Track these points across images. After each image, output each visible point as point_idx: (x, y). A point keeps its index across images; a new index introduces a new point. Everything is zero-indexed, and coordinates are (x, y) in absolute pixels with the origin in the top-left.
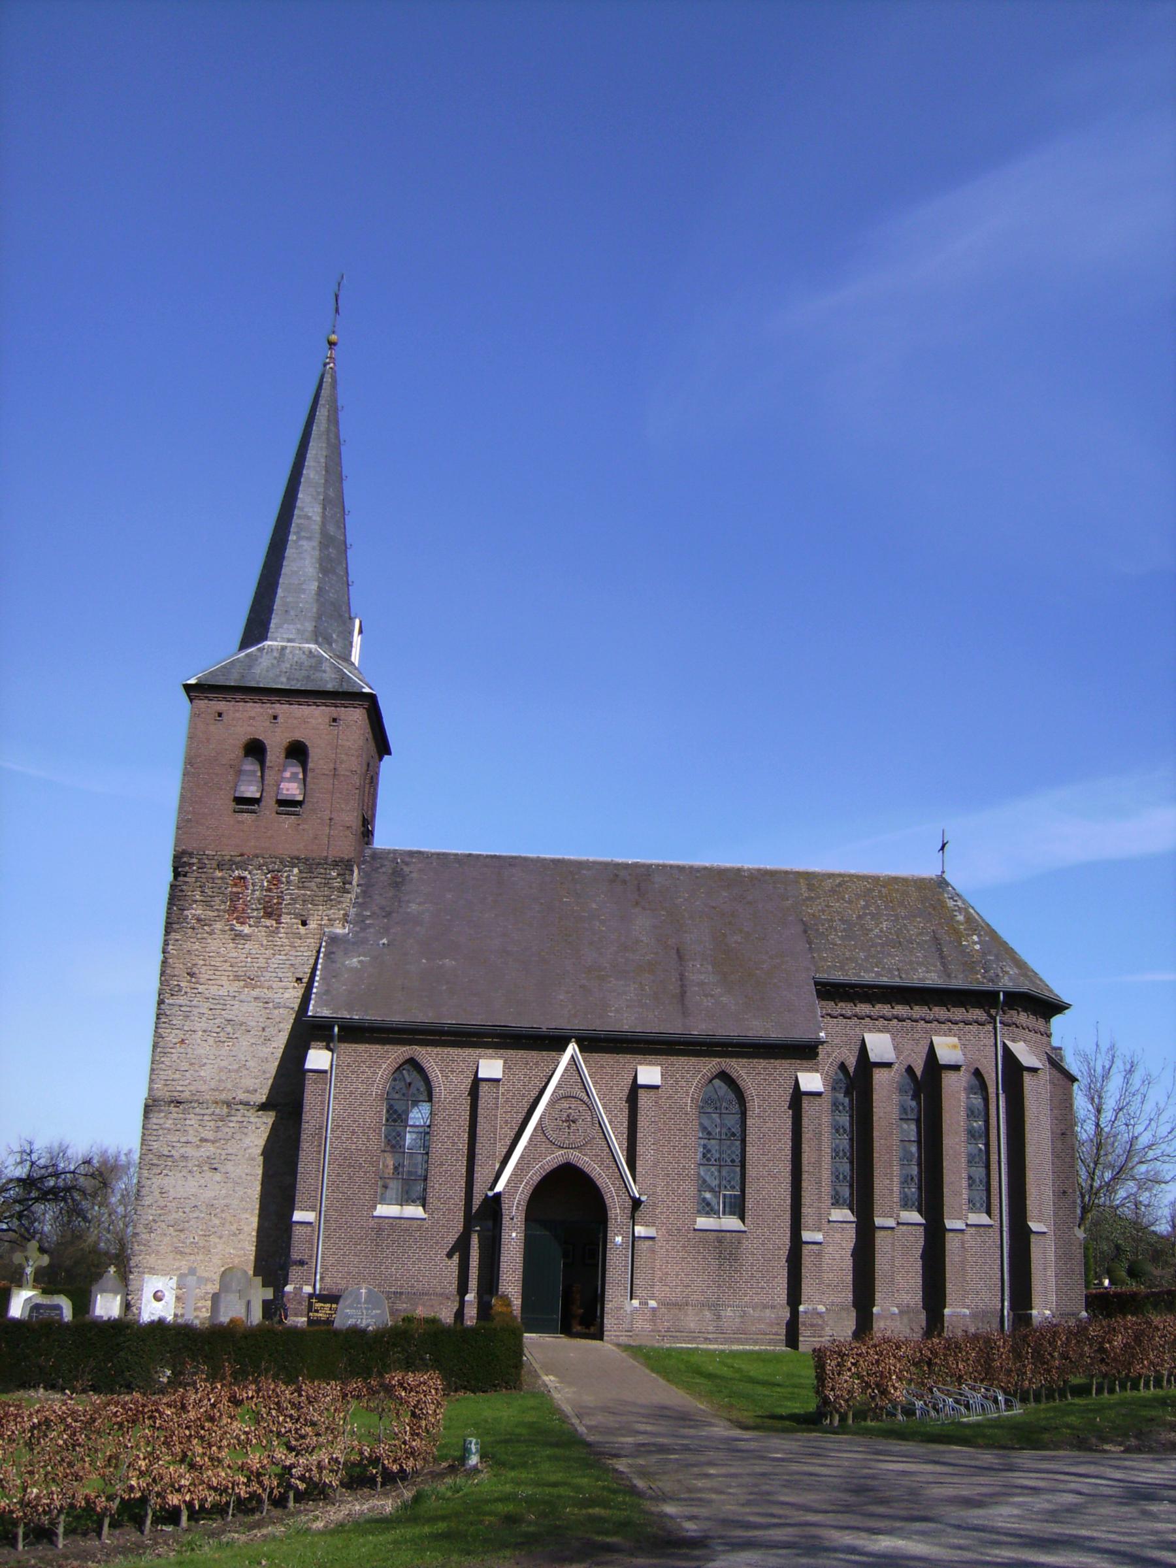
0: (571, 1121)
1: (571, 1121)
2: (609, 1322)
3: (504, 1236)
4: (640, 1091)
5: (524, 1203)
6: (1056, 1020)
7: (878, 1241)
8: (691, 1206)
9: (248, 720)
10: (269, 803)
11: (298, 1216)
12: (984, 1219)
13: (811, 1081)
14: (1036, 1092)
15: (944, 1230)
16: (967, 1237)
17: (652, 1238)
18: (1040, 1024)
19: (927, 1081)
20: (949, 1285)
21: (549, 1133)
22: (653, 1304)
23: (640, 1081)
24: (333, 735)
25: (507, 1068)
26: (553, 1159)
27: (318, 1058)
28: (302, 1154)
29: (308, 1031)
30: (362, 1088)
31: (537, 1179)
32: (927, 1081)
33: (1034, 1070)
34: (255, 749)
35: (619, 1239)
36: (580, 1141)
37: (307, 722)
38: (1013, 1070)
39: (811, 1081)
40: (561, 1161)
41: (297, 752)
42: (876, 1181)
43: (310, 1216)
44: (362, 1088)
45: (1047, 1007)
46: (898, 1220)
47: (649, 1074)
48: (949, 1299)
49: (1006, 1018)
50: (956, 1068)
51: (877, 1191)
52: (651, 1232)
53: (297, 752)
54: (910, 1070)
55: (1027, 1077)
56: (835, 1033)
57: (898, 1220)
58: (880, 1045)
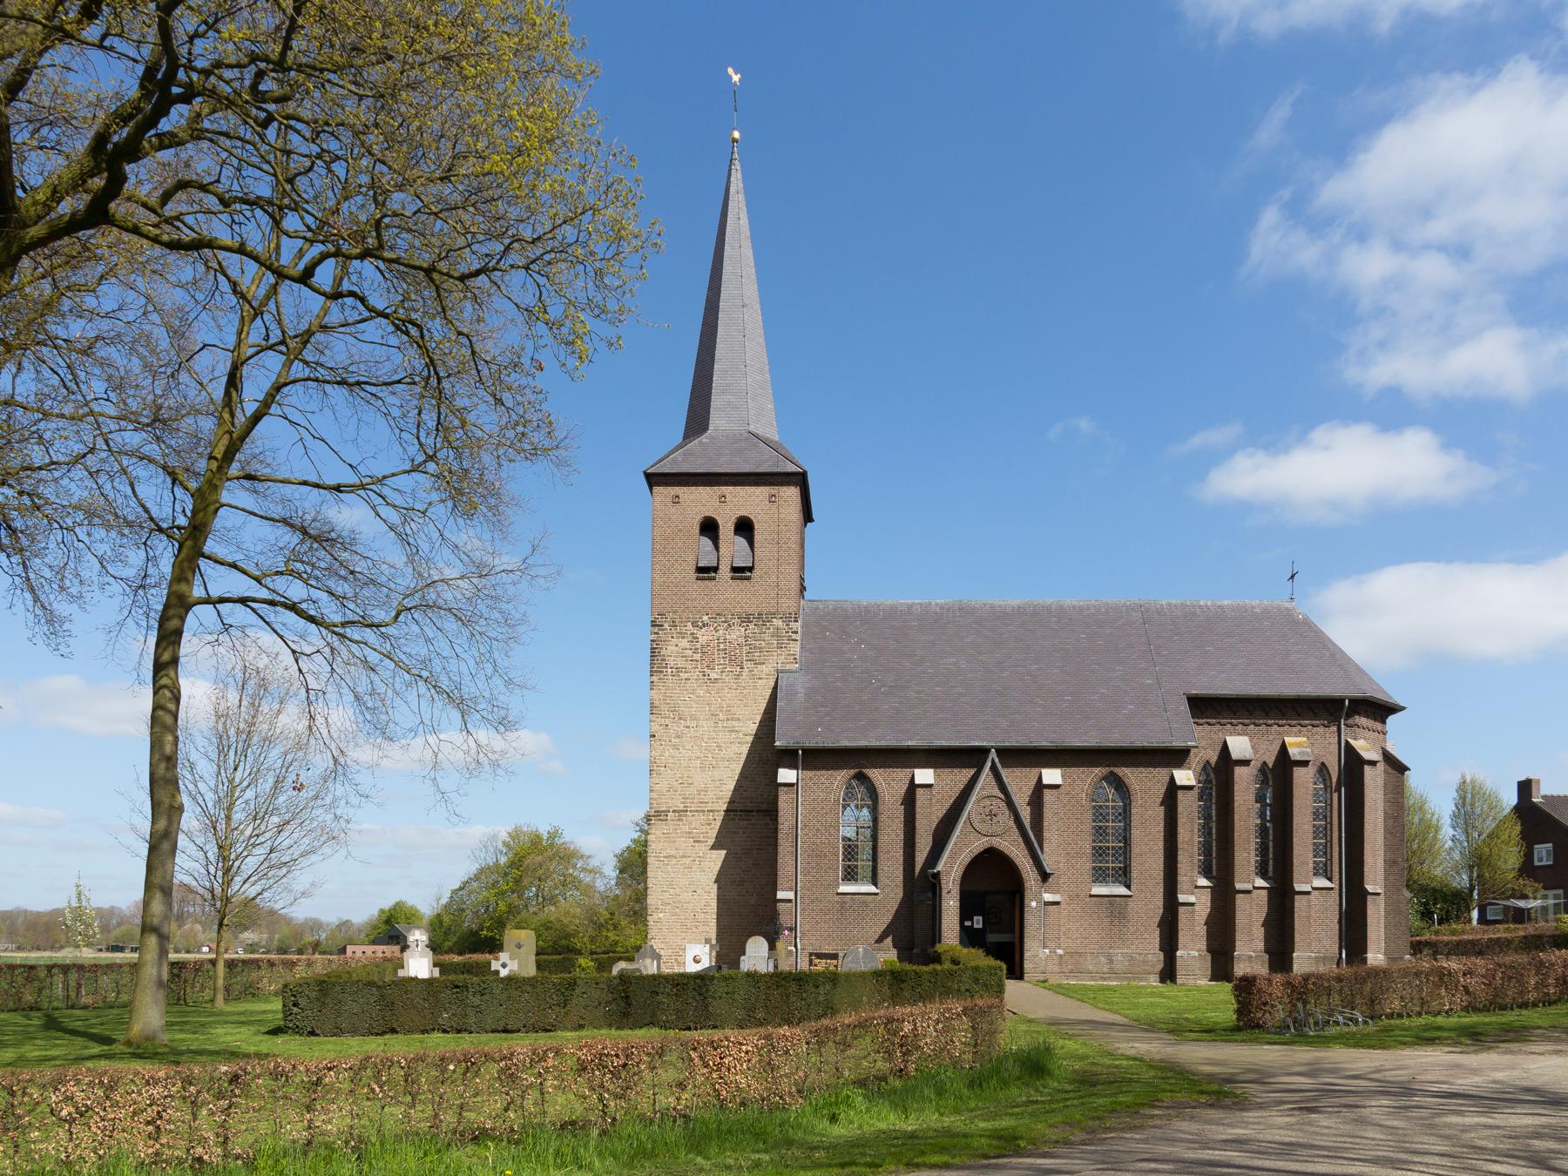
0: (992, 815)
1: (992, 815)
2: (1027, 965)
3: (944, 904)
4: (1046, 792)
5: (958, 880)
6: (1391, 719)
7: (1297, 904)
8: (1087, 877)
9: (702, 501)
10: (725, 571)
11: (780, 895)
12: (1327, 884)
13: (1184, 777)
14: (1374, 779)
15: (1365, 893)
16: (1312, 897)
17: (1057, 903)
18: (1378, 726)
19: (1281, 770)
20: (1297, 935)
21: (976, 825)
22: (1060, 952)
23: (1046, 781)
24: (771, 509)
25: (937, 776)
26: (979, 845)
27: (786, 775)
28: (780, 849)
29: (767, 754)
30: (823, 795)
31: (968, 860)
32: (1281, 770)
33: (1373, 763)
34: (709, 528)
35: (1034, 904)
36: (999, 830)
37: (748, 501)
38: (1354, 765)
39: (1184, 777)
40: (987, 846)
41: (745, 527)
42: (1237, 854)
43: (790, 895)
44: (823, 795)
45: (1380, 710)
46: (1252, 885)
47: (1052, 776)
48: (1297, 946)
49: (1350, 721)
50: (1305, 763)
51: (1237, 862)
52: (1057, 898)
53: (745, 527)
54: (1323, 769)
55: (1367, 768)
56: (1203, 740)
57: (1252, 885)
58: (1239, 745)
